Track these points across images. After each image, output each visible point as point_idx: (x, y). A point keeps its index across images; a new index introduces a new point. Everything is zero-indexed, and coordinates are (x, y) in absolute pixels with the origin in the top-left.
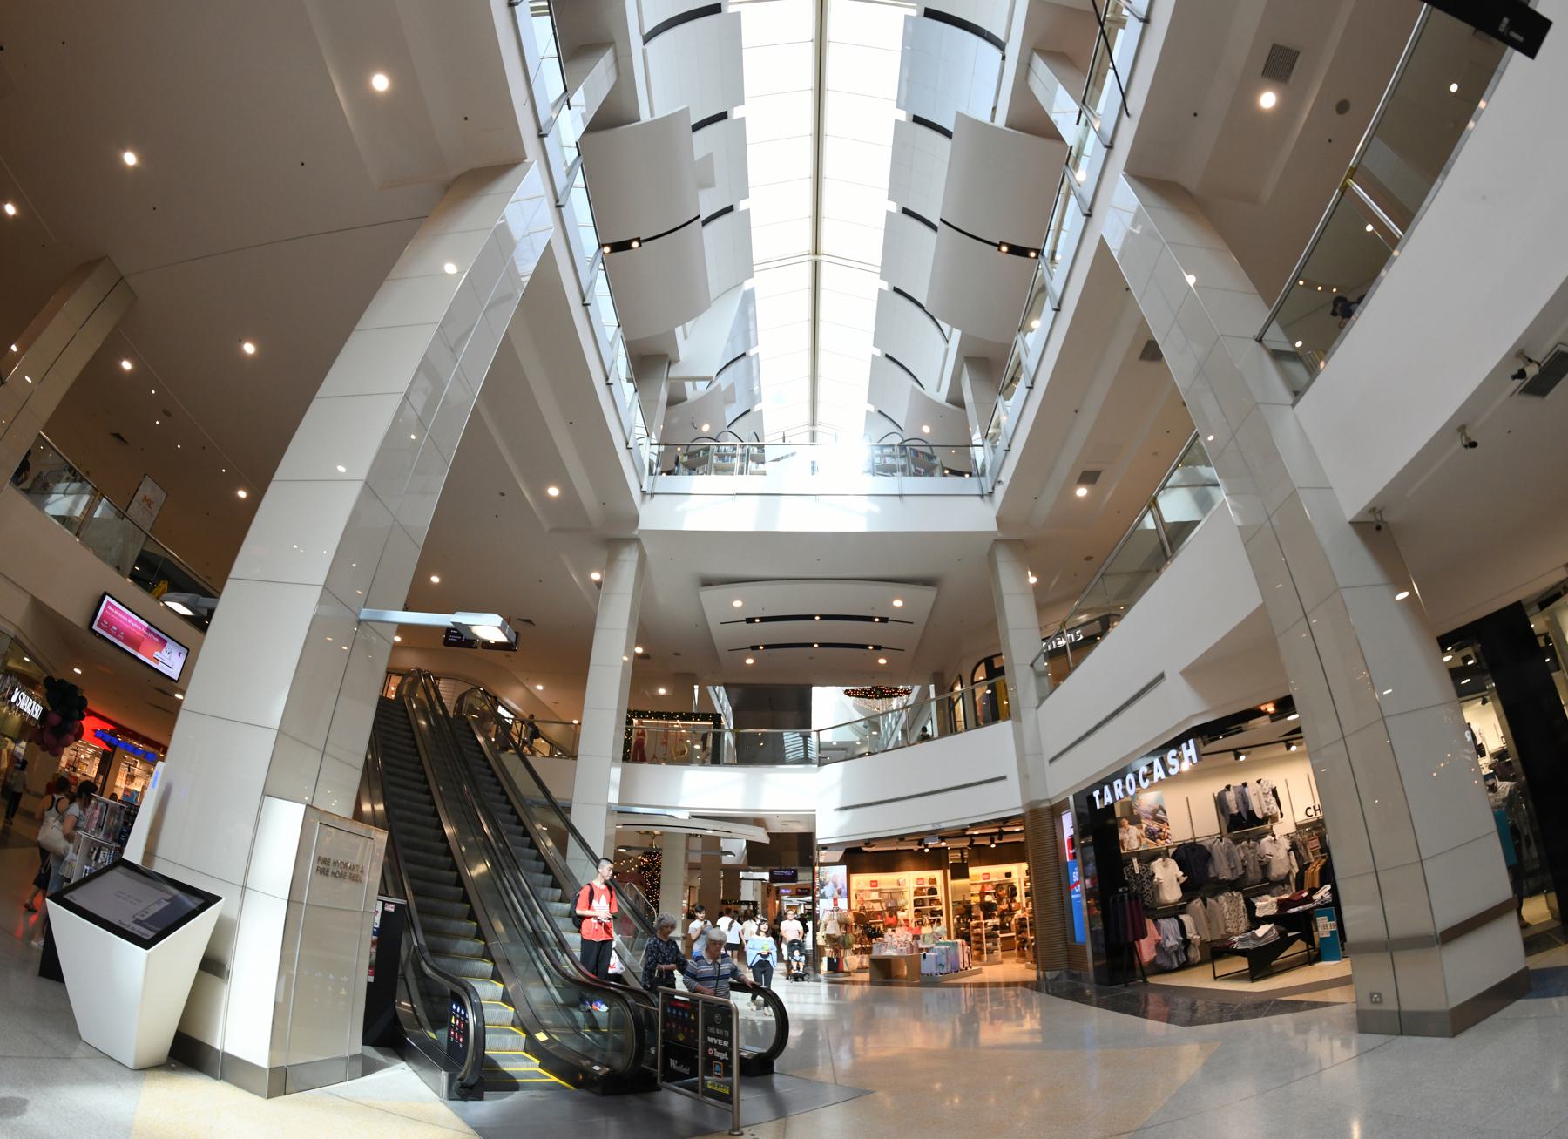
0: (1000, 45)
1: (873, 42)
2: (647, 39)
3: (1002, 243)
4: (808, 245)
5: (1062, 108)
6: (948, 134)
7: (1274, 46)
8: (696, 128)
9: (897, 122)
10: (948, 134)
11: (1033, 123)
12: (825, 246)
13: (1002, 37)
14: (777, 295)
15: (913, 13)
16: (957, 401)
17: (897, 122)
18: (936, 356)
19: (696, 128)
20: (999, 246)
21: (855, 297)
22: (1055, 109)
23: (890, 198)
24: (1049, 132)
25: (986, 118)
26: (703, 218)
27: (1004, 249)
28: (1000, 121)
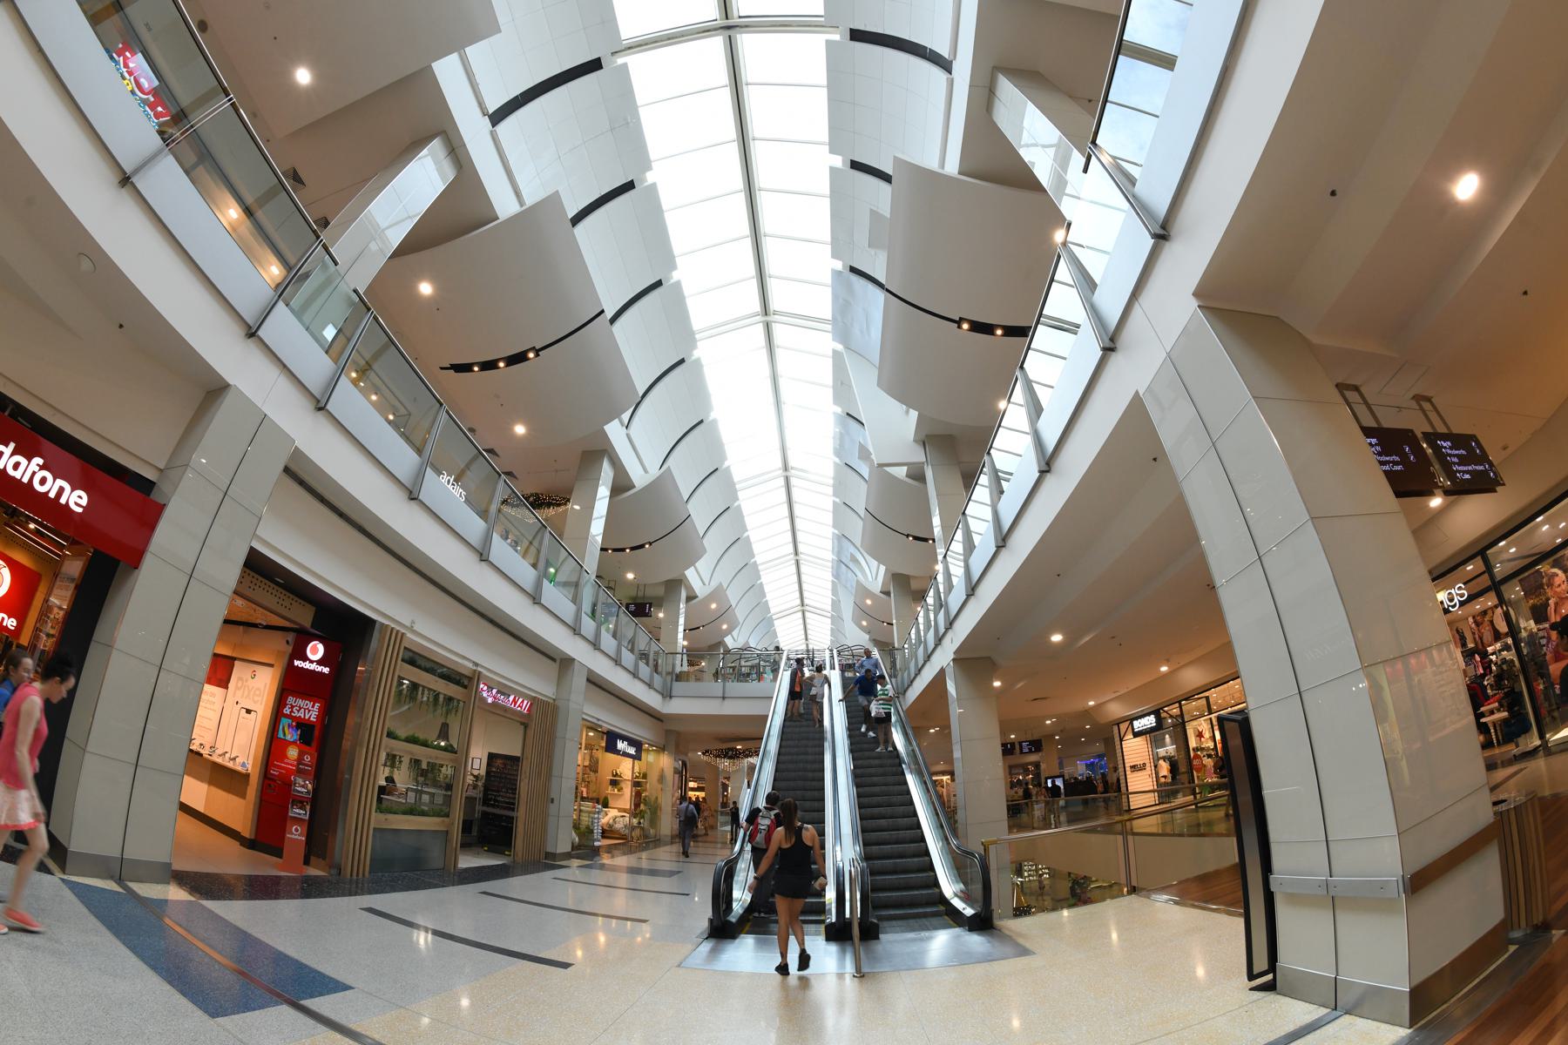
0: (945, 65)
1: (793, 75)
2: (497, 117)
3: (961, 319)
4: (756, 306)
5: (1034, 134)
6: (887, 178)
7: (499, 31)
8: (576, 220)
9: (832, 169)
10: (887, 178)
11: (998, 168)
12: (774, 305)
13: (945, 52)
14: (728, 369)
15: (836, 37)
16: (918, 476)
17: (832, 169)
18: (895, 428)
19: (576, 220)
20: (959, 323)
21: (810, 355)
22: (1026, 138)
23: (834, 256)
24: (1022, 179)
25: (932, 164)
26: (609, 314)
27: (965, 326)
28: (952, 167)
